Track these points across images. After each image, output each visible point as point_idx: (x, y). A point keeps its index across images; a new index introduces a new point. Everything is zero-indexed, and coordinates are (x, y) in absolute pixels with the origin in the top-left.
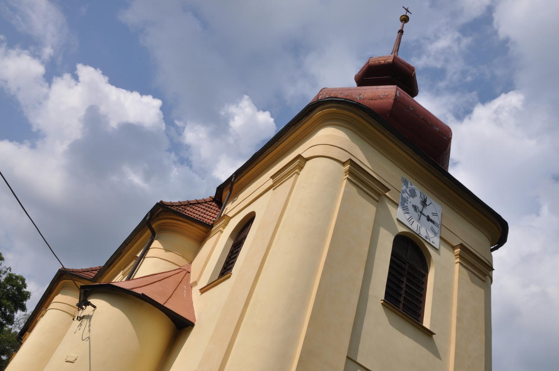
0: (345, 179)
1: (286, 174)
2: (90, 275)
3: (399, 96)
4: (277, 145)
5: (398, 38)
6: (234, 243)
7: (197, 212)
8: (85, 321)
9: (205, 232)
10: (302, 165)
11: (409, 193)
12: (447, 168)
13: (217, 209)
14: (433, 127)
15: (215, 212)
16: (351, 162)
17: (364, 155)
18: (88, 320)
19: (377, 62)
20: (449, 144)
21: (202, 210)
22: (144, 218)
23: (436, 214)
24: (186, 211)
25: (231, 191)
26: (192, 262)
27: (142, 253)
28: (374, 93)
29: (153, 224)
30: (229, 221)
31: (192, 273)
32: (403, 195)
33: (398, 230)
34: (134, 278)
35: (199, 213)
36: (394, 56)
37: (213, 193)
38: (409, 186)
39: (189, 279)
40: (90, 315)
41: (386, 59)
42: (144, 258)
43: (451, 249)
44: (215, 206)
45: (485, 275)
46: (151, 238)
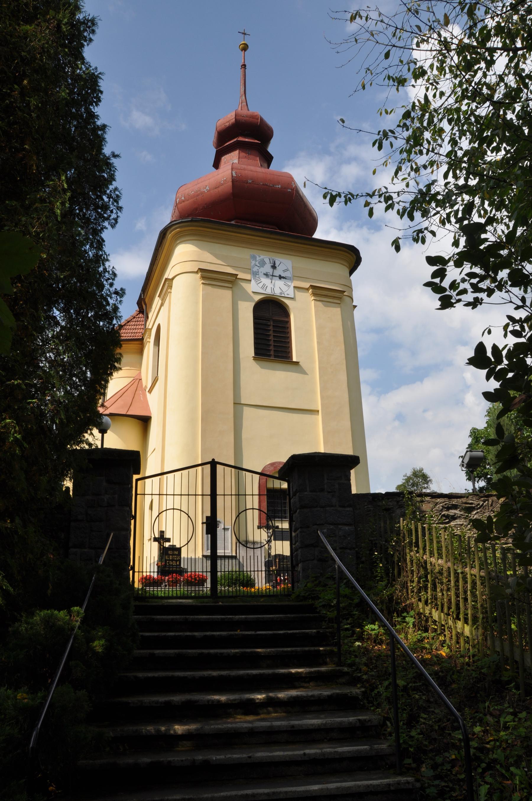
7: (129, 331)
9: (139, 344)
11: (258, 265)
19: (223, 126)
21: (133, 327)
31: (143, 379)
35: (131, 331)
37: (137, 309)
38: (258, 258)
39: (142, 385)
43: (306, 291)
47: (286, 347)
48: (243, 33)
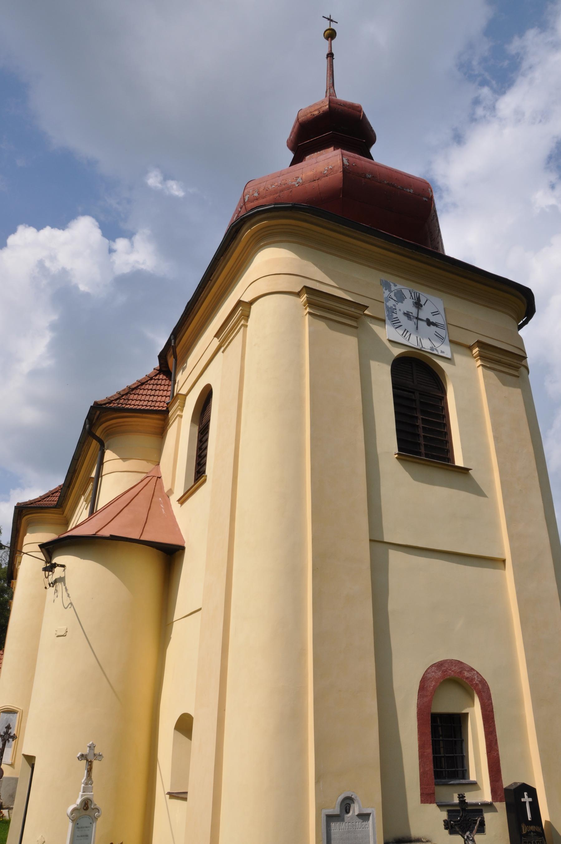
0: (306, 315)
1: (231, 328)
2: (52, 500)
3: (348, 164)
4: (211, 285)
5: (329, 66)
6: (199, 428)
7: (143, 398)
8: (59, 586)
10: (246, 313)
12: (438, 235)
13: (167, 382)
14: (405, 189)
15: (166, 388)
16: (307, 289)
17: (321, 270)
18: (62, 583)
19: (309, 115)
20: (432, 204)
21: (149, 392)
22: (84, 426)
23: (437, 312)
24: (130, 402)
25: (175, 357)
26: (159, 462)
27: (97, 467)
28: (314, 171)
29: (96, 432)
30: (185, 400)
31: (163, 478)
32: (388, 304)
33: (393, 355)
34: (98, 510)
35: (147, 398)
36: (328, 100)
37: (157, 364)
38: (393, 288)
39: (162, 487)
40: (61, 577)
41: (319, 107)
42: (102, 476)
43: (467, 351)
44: (165, 379)
45: (517, 368)
46: (100, 450)
47: (443, 441)
48: (328, 19)
